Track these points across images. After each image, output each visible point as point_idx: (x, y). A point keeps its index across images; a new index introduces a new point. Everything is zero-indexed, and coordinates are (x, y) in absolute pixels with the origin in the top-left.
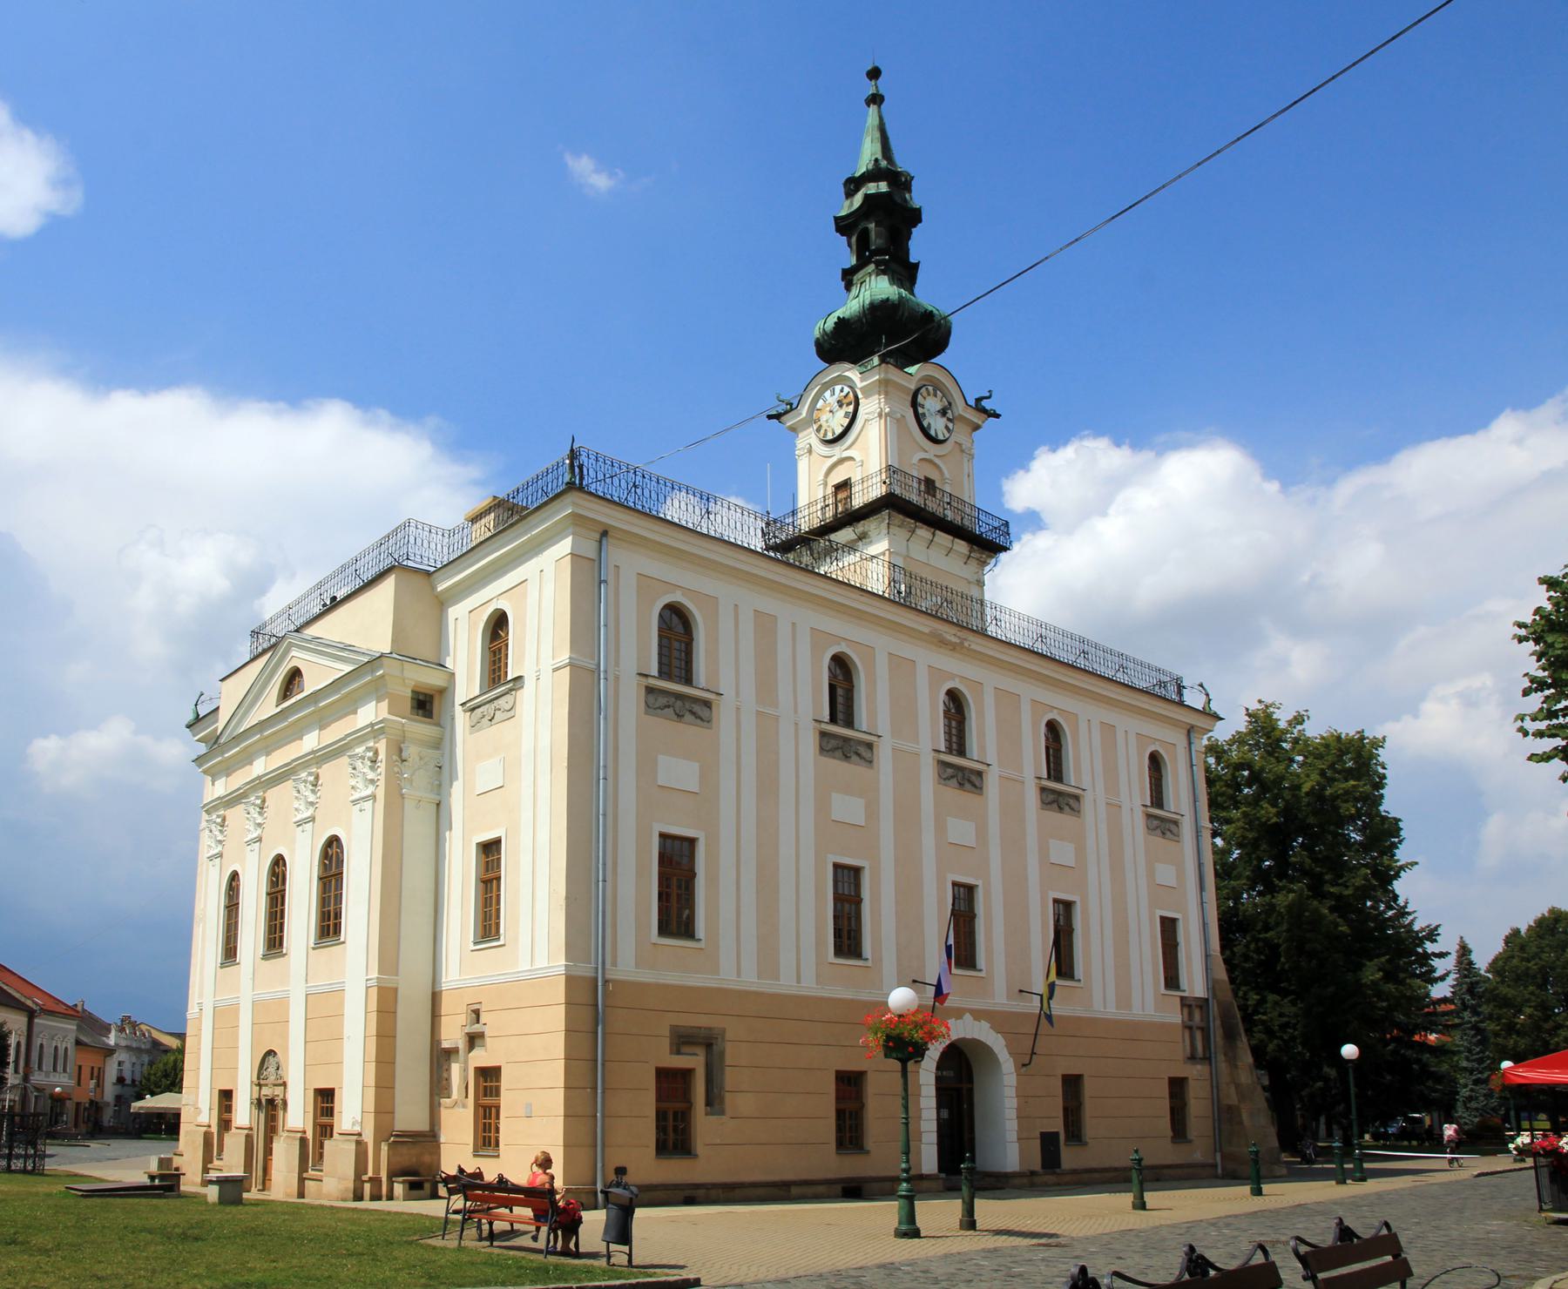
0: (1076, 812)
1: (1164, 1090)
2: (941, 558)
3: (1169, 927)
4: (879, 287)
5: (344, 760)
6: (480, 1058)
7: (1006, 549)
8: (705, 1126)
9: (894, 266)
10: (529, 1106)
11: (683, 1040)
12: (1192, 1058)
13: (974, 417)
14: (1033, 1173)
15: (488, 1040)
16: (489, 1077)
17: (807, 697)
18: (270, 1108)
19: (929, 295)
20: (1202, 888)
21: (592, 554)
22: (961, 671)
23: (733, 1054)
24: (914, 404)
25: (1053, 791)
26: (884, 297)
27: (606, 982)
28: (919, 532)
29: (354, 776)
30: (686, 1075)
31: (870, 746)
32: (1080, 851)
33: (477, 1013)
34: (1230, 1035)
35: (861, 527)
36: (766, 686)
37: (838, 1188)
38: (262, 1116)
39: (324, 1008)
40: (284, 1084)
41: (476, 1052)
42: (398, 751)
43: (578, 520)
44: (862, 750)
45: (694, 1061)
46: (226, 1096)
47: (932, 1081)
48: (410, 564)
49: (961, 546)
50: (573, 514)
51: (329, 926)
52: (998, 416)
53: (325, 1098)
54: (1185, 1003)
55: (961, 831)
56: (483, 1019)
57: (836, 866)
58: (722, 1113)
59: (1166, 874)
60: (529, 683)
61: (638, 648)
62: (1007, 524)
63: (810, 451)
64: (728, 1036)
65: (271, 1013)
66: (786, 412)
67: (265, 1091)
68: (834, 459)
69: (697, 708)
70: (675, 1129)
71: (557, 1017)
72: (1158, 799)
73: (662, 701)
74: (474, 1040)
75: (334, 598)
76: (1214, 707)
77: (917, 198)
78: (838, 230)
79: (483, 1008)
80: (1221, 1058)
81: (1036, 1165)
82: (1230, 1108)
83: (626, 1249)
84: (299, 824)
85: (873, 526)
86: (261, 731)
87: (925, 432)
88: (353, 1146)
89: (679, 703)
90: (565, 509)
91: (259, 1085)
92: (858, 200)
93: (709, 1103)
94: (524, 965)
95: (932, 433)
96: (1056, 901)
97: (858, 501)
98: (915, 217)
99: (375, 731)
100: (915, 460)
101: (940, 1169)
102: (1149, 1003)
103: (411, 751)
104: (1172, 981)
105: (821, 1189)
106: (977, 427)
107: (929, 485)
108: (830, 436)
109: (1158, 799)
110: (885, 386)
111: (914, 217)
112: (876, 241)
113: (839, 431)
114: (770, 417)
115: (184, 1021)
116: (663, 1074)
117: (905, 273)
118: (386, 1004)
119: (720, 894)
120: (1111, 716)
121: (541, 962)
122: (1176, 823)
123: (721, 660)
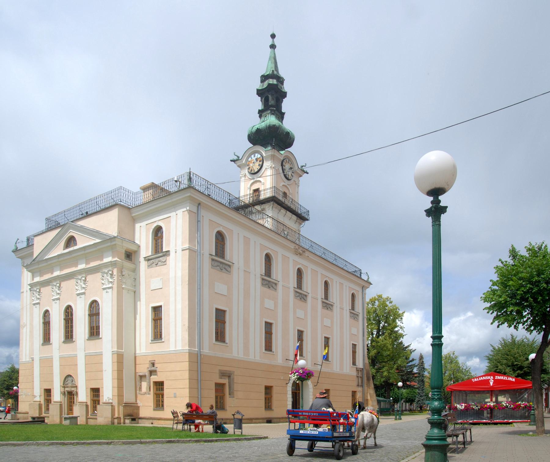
0: (331, 310)
1: (263, 390)
2: (289, 220)
3: (354, 346)
4: (272, 120)
5: (99, 275)
6: (154, 378)
7: (308, 220)
9: (276, 112)
10: (175, 394)
11: (223, 374)
12: (358, 385)
13: (300, 172)
15: (158, 373)
16: (160, 385)
17: (259, 267)
18: (71, 395)
19: (288, 125)
20: (363, 336)
21: (196, 211)
22: (302, 262)
23: (237, 379)
24: (282, 165)
26: (274, 124)
27: (201, 355)
29: (103, 280)
30: (223, 385)
31: (276, 284)
32: (332, 323)
33: (153, 365)
34: (368, 379)
35: (263, 206)
37: (265, 421)
38: (66, 398)
39: (94, 361)
40: (76, 387)
41: (152, 377)
42: (121, 274)
43: (192, 199)
44: (274, 285)
45: (225, 381)
46: (48, 392)
47: (291, 390)
48: (122, 203)
49: (294, 217)
50: (190, 196)
51: (94, 332)
52: (308, 173)
53: (96, 392)
54: (358, 370)
55: (300, 313)
56: (156, 365)
57: (266, 322)
58: (233, 397)
59: (354, 331)
60: (172, 254)
61: (209, 246)
63: (245, 176)
64: (235, 373)
66: (237, 160)
67: (67, 389)
69: (227, 267)
70: (220, 402)
71: (186, 365)
72: (353, 308)
73: (216, 264)
74: (152, 373)
75: (87, 213)
76: (370, 280)
77: (286, 87)
78: (257, 94)
79: (156, 362)
80: (365, 385)
83: (240, 430)
84: (78, 295)
85: (267, 207)
86: (58, 258)
87: (285, 176)
88: (110, 407)
89: (221, 265)
90: (188, 194)
91: (64, 387)
92: (266, 84)
94: (172, 348)
96: (325, 337)
97: (262, 197)
98: (284, 95)
99: (113, 264)
100: (281, 185)
102: (348, 370)
103: (125, 272)
104: (354, 363)
105: (261, 421)
106: (301, 176)
107: (285, 194)
109: (353, 308)
110: (273, 158)
111: (284, 95)
112: (272, 102)
113: (256, 170)
114: (231, 161)
115: (77, 362)
116: (217, 384)
117: (281, 116)
118: (120, 359)
119: (233, 329)
120: (342, 281)
121: (179, 348)
122: (358, 315)
123: (234, 250)
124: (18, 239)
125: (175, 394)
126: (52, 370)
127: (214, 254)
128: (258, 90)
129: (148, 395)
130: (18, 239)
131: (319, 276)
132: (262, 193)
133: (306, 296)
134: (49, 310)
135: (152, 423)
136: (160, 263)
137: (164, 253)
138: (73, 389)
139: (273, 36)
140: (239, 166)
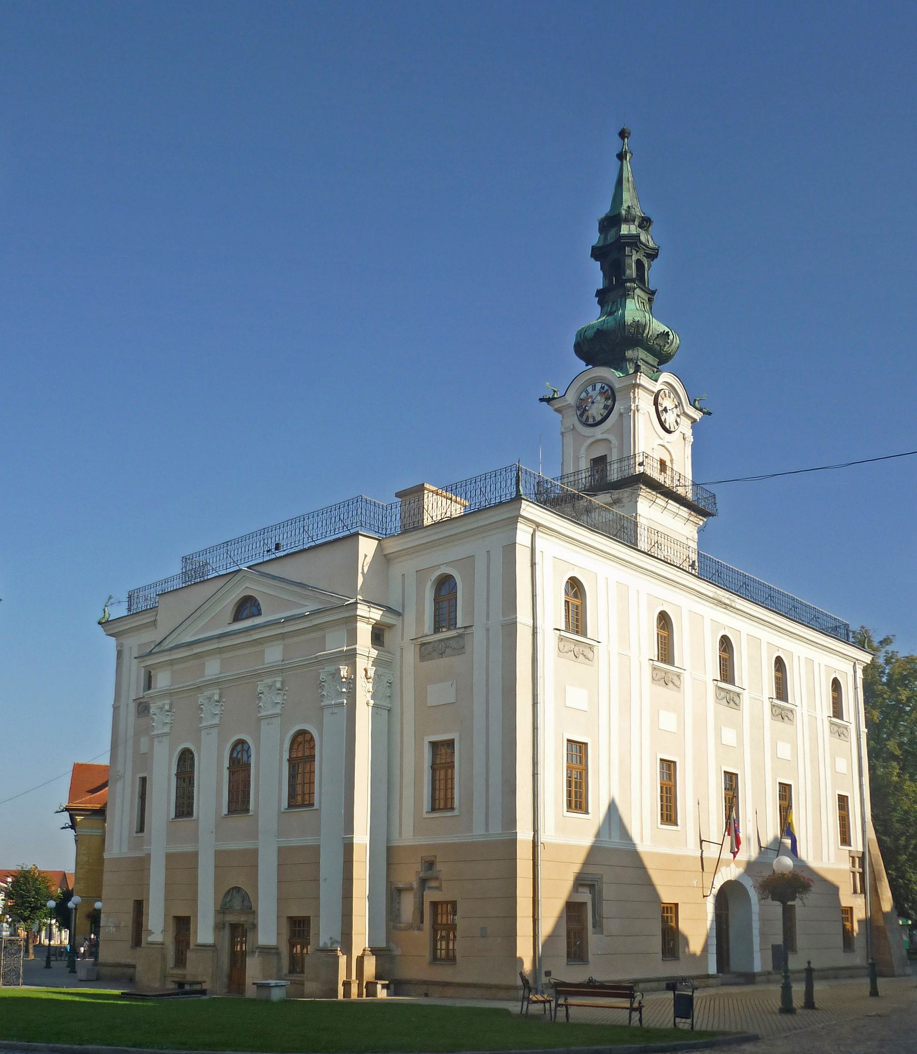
3: (843, 801)
6: (431, 896)
7: (712, 515)
8: (594, 941)
10: (484, 929)
12: (855, 892)
14: (769, 973)
23: (608, 892)
24: (656, 403)
25: (779, 707)
28: (658, 501)
36: (814, 739)
37: (664, 984)
49: (684, 511)
62: (714, 496)
65: (238, 865)
66: (554, 399)
68: (592, 440)
81: (770, 967)
82: (878, 928)
83: (689, 1021)
85: (626, 495)
93: (594, 927)
95: (668, 426)
101: (718, 971)
104: (845, 839)
105: (654, 985)
108: (591, 421)
113: (599, 418)
114: (542, 400)
124: (110, 598)
125: (484, 929)
126: (196, 877)
127: (564, 628)
128: (593, 248)
129: (416, 932)
130: (110, 598)
131: (764, 647)
132: (615, 466)
133: (738, 695)
134: (193, 748)
135: (426, 995)
136: (448, 651)
137: (460, 631)
138: (243, 919)
139: (623, 134)
140: (557, 410)
